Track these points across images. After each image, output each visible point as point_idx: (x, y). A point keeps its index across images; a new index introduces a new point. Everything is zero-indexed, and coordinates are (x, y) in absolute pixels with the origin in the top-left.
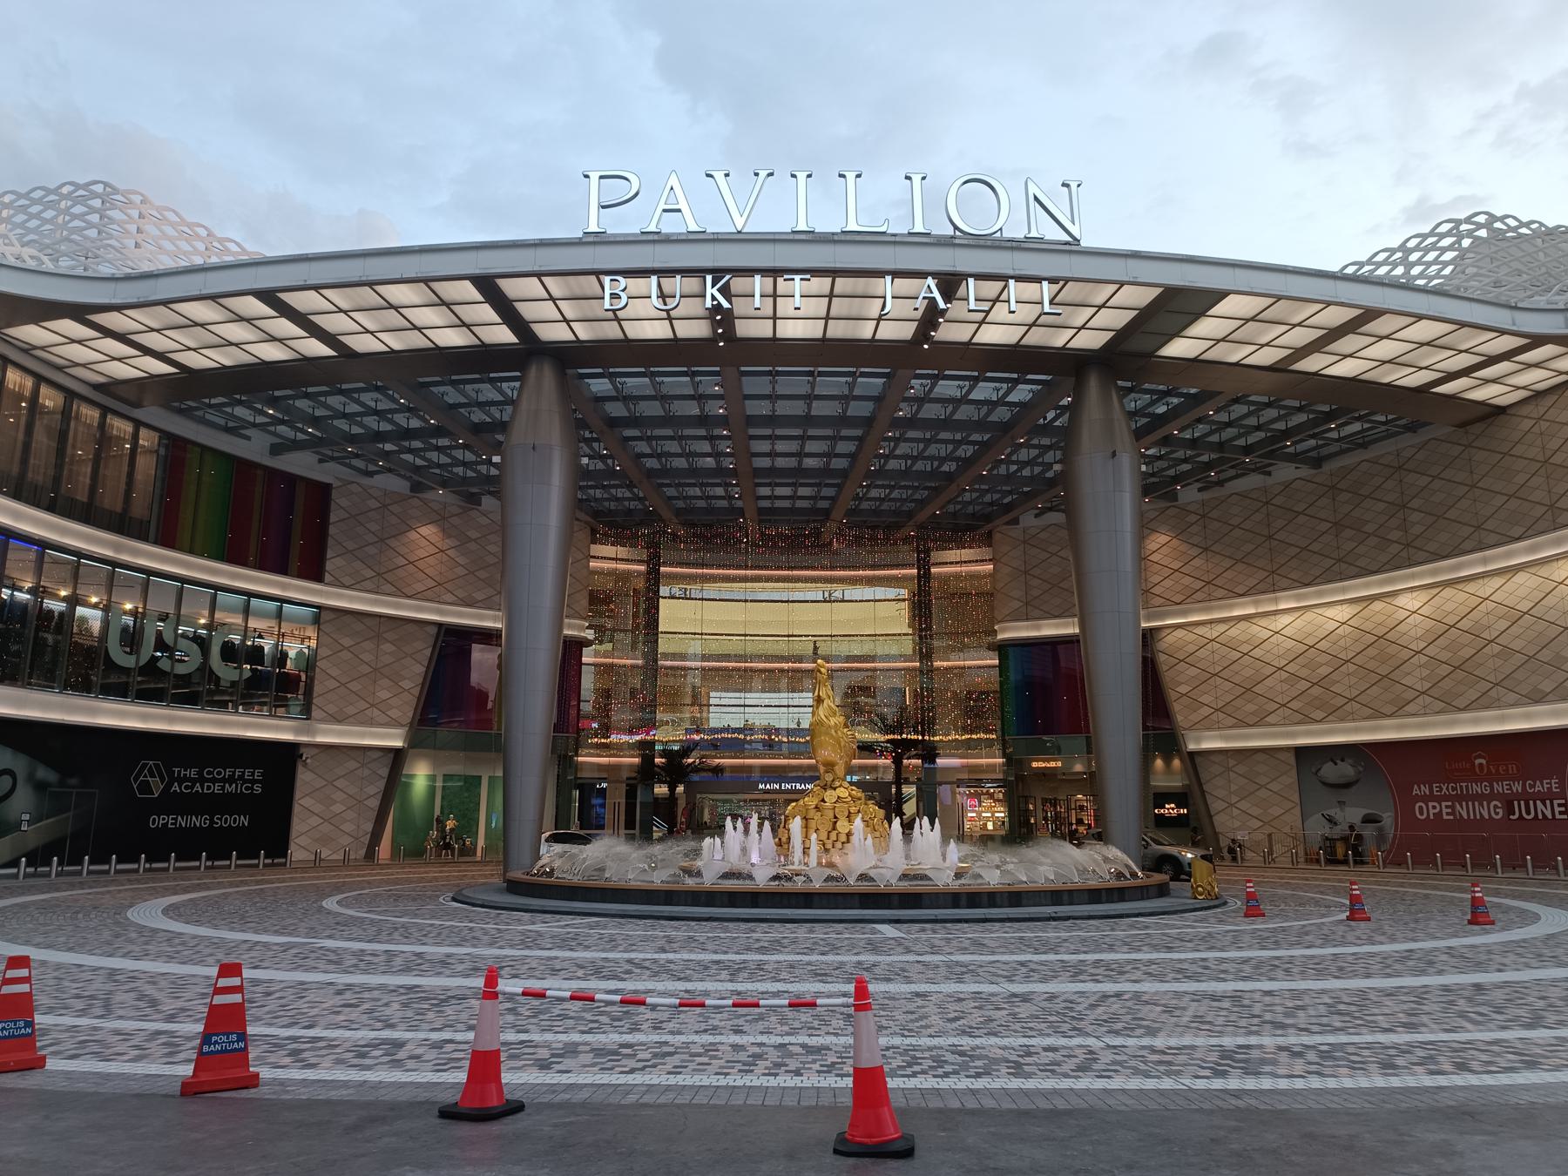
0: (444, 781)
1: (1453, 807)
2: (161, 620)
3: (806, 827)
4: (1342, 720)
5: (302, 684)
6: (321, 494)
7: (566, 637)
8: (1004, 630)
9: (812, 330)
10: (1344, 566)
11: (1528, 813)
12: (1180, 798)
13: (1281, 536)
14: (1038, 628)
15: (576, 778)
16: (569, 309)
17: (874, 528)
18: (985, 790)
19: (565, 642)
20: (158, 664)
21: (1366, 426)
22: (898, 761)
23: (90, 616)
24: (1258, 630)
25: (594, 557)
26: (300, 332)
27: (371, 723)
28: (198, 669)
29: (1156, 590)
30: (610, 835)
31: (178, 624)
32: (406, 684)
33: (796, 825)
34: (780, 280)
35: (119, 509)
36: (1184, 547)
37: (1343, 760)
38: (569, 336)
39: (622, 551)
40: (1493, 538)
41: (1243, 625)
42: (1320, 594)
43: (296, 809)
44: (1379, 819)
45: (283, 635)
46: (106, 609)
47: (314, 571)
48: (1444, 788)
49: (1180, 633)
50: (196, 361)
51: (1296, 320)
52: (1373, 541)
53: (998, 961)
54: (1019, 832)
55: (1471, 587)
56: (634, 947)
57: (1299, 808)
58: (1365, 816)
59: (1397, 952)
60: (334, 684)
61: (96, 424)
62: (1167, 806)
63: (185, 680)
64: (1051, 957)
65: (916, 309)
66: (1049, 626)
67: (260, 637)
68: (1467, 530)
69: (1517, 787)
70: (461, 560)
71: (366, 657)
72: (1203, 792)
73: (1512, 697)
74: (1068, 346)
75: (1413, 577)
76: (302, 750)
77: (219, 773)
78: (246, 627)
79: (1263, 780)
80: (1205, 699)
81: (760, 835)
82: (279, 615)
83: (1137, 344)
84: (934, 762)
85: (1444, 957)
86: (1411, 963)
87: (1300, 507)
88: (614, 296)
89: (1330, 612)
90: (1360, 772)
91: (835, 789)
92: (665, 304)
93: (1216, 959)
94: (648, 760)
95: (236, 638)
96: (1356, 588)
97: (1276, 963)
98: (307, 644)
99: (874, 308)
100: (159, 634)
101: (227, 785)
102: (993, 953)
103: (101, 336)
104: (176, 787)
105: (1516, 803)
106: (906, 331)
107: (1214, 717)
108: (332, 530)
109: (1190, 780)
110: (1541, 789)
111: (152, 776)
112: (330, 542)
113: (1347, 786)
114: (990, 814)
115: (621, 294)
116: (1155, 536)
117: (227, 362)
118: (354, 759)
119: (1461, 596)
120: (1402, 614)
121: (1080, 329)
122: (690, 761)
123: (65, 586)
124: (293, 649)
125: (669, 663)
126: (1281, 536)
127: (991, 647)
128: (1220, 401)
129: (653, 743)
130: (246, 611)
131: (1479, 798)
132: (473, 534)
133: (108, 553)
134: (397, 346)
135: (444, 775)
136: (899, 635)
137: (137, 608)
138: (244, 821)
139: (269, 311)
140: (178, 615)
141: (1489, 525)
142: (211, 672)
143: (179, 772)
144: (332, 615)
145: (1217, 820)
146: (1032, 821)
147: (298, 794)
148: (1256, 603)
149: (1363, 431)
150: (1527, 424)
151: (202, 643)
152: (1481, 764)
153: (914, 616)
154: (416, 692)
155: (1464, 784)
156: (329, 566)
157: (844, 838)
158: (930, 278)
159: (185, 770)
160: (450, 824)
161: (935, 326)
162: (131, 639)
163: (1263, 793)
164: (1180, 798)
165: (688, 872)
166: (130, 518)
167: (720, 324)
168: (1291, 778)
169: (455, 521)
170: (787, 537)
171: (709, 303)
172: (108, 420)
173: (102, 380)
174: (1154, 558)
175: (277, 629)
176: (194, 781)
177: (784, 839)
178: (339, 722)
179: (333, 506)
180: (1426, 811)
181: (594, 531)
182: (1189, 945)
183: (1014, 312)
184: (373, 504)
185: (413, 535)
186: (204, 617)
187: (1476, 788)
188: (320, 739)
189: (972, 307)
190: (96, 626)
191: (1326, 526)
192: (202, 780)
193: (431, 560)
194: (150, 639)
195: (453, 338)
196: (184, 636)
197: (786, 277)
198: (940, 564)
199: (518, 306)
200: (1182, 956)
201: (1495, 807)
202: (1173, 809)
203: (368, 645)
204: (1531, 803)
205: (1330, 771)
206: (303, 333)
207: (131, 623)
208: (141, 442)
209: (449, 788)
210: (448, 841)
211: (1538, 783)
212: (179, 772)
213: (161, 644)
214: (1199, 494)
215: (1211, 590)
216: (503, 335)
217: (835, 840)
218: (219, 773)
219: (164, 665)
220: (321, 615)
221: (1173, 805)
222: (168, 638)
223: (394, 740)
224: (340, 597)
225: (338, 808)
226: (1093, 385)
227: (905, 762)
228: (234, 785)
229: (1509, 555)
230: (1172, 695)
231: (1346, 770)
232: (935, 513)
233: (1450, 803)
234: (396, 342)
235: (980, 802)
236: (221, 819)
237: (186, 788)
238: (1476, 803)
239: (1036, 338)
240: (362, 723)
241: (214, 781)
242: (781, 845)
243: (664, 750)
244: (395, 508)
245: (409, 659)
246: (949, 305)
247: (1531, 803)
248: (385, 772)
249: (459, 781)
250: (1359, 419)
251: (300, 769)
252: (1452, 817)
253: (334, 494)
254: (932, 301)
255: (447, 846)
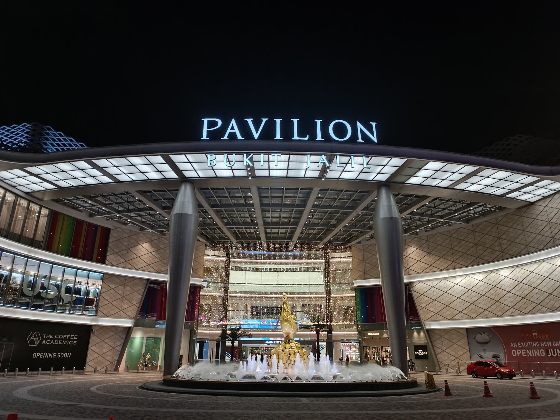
0: (147, 340)
1: (526, 351)
2: (44, 278)
3: (279, 358)
4: (483, 318)
5: (95, 303)
6: (106, 232)
7: (191, 284)
8: (356, 283)
9: (283, 173)
10: (479, 260)
11: (554, 354)
12: (424, 348)
13: (456, 248)
14: (369, 282)
15: (197, 339)
16: (196, 166)
17: (308, 244)
18: (352, 344)
19: (191, 286)
20: (41, 295)
21: (484, 208)
22: (318, 333)
23: (17, 277)
24: (449, 284)
25: (206, 255)
26: (100, 174)
27: (120, 317)
28: (56, 297)
29: (412, 268)
30: (207, 362)
31: (50, 280)
32: (134, 302)
33: (275, 357)
34: (270, 156)
35: (32, 237)
36: (421, 252)
37: (484, 333)
38: (196, 176)
39: (216, 253)
40: (533, 250)
41: (444, 281)
42: (471, 270)
43: (89, 351)
44: (498, 356)
45: (89, 284)
46: (24, 274)
47: (102, 260)
48: (522, 344)
49: (421, 284)
50: (63, 184)
51: (455, 171)
52: (489, 250)
53: (342, 414)
54: (364, 359)
55: (526, 268)
56: (202, 407)
57: (468, 352)
58: (494, 355)
59: (499, 410)
60: (107, 302)
61: (26, 206)
62: (419, 351)
63: (52, 300)
64: (364, 412)
65: (318, 166)
66: (373, 281)
67: (80, 284)
68: (523, 247)
69: (549, 344)
70: (157, 256)
71: (120, 292)
72: (433, 345)
73: (545, 309)
74: (374, 180)
75: (505, 264)
76: (93, 328)
77: (61, 337)
78: (75, 281)
79: (455, 341)
80: (431, 309)
81: (243, 366)
82: (88, 277)
83: (399, 179)
84: (332, 333)
85: (517, 412)
86: (503, 415)
87: (462, 238)
88: (211, 161)
89: (476, 277)
90: (490, 338)
91: (290, 343)
92: (230, 164)
93: (428, 413)
94: (224, 332)
95: (71, 285)
96: (485, 268)
97: (451, 415)
98: (98, 287)
99: (304, 166)
100: (42, 284)
101: (64, 341)
102: (342, 410)
103: (30, 175)
104: (44, 342)
105: (549, 350)
106: (316, 174)
107: (435, 316)
108: (110, 245)
109: (427, 341)
110: (558, 345)
111: (35, 337)
112: (109, 249)
113: (486, 343)
114: (353, 353)
115: (213, 160)
116: (410, 248)
117: (74, 185)
118: (113, 331)
119: (523, 271)
120: (502, 278)
121: (378, 173)
122: (240, 332)
123: (9, 265)
124: (92, 289)
125: (232, 295)
126: (456, 248)
127: (352, 289)
128: (430, 199)
129: (226, 325)
130: (76, 275)
131: (536, 348)
132: (162, 246)
133: (26, 253)
134: (135, 179)
135: (147, 338)
136: (318, 284)
137: (35, 273)
138: (69, 355)
139: (89, 167)
140: (50, 276)
141: (531, 245)
142: (61, 298)
143: (46, 336)
144: (108, 276)
145: (439, 356)
146: (369, 356)
147: (90, 345)
148: (448, 273)
149: (483, 210)
150: (542, 208)
151: (58, 287)
152: (535, 335)
153: (326, 278)
154: (138, 305)
155: (530, 343)
156: (108, 258)
157: (292, 363)
158: (323, 155)
159: (48, 335)
160: (148, 357)
161: (326, 172)
162: (32, 285)
163: (455, 346)
164: (424, 348)
165: (231, 375)
166: (36, 240)
167: (249, 171)
168: (465, 340)
169: (155, 242)
170: (277, 248)
171: (245, 164)
172: (30, 205)
173: (29, 191)
174: (410, 256)
175: (87, 282)
176: (51, 340)
177: (270, 363)
178: (108, 317)
179: (111, 236)
180: (516, 353)
181: (206, 246)
182: (420, 407)
183: (353, 167)
184: (126, 235)
185: (140, 247)
186: (60, 277)
187: (534, 344)
188: (100, 323)
189: (338, 165)
190: (19, 281)
191: (472, 245)
192: (54, 339)
193: (146, 256)
194: (39, 285)
195: (155, 176)
196: (52, 284)
197: (272, 155)
198: (333, 258)
199: (177, 164)
200: (416, 412)
201: (542, 352)
202: (421, 352)
203: (121, 287)
204: (555, 350)
205: (480, 338)
206: (101, 174)
207: (32, 280)
208: (42, 213)
209: (148, 342)
210: (147, 363)
211: (557, 342)
212: (46, 336)
213: (43, 287)
214: (426, 232)
215: (431, 269)
216: (172, 175)
217: (289, 362)
218: (61, 337)
219: (43, 295)
220: (105, 277)
221: (421, 351)
222: (46, 285)
223: (128, 323)
224: (111, 270)
225: (105, 350)
226: (384, 193)
227: (320, 333)
228: (66, 341)
229: (539, 256)
230: (419, 308)
231: (485, 337)
232: (330, 239)
233: (525, 350)
234: (134, 177)
235: (350, 348)
236: (60, 355)
237: (48, 342)
238: (535, 350)
239: (362, 177)
240: (116, 317)
241: (59, 339)
242: (269, 365)
243: (230, 328)
244: (134, 237)
245: (136, 292)
246: (330, 165)
247: (555, 350)
248: (124, 336)
249: (153, 339)
250: (481, 206)
251: (92, 335)
252: (526, 356)
253: (112, 232)
254: (324, 163)
255: (146, 365)
